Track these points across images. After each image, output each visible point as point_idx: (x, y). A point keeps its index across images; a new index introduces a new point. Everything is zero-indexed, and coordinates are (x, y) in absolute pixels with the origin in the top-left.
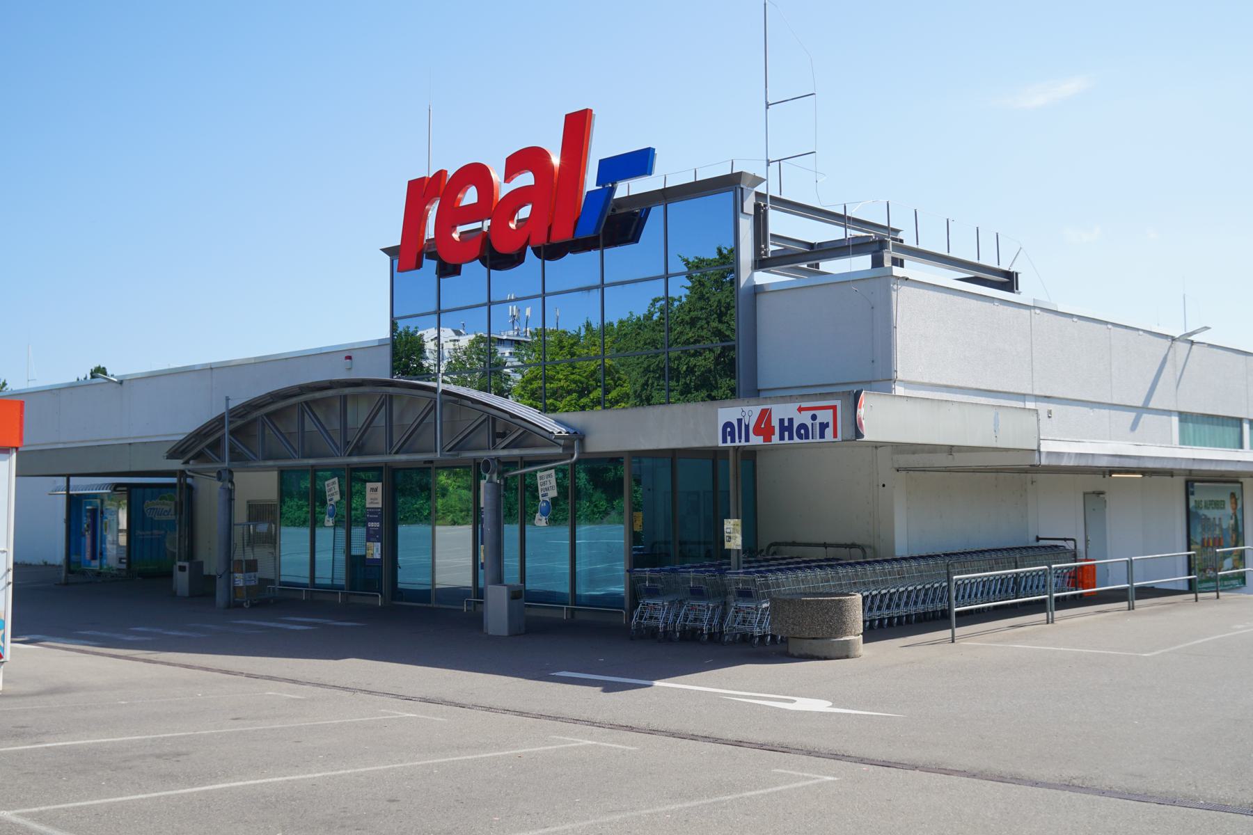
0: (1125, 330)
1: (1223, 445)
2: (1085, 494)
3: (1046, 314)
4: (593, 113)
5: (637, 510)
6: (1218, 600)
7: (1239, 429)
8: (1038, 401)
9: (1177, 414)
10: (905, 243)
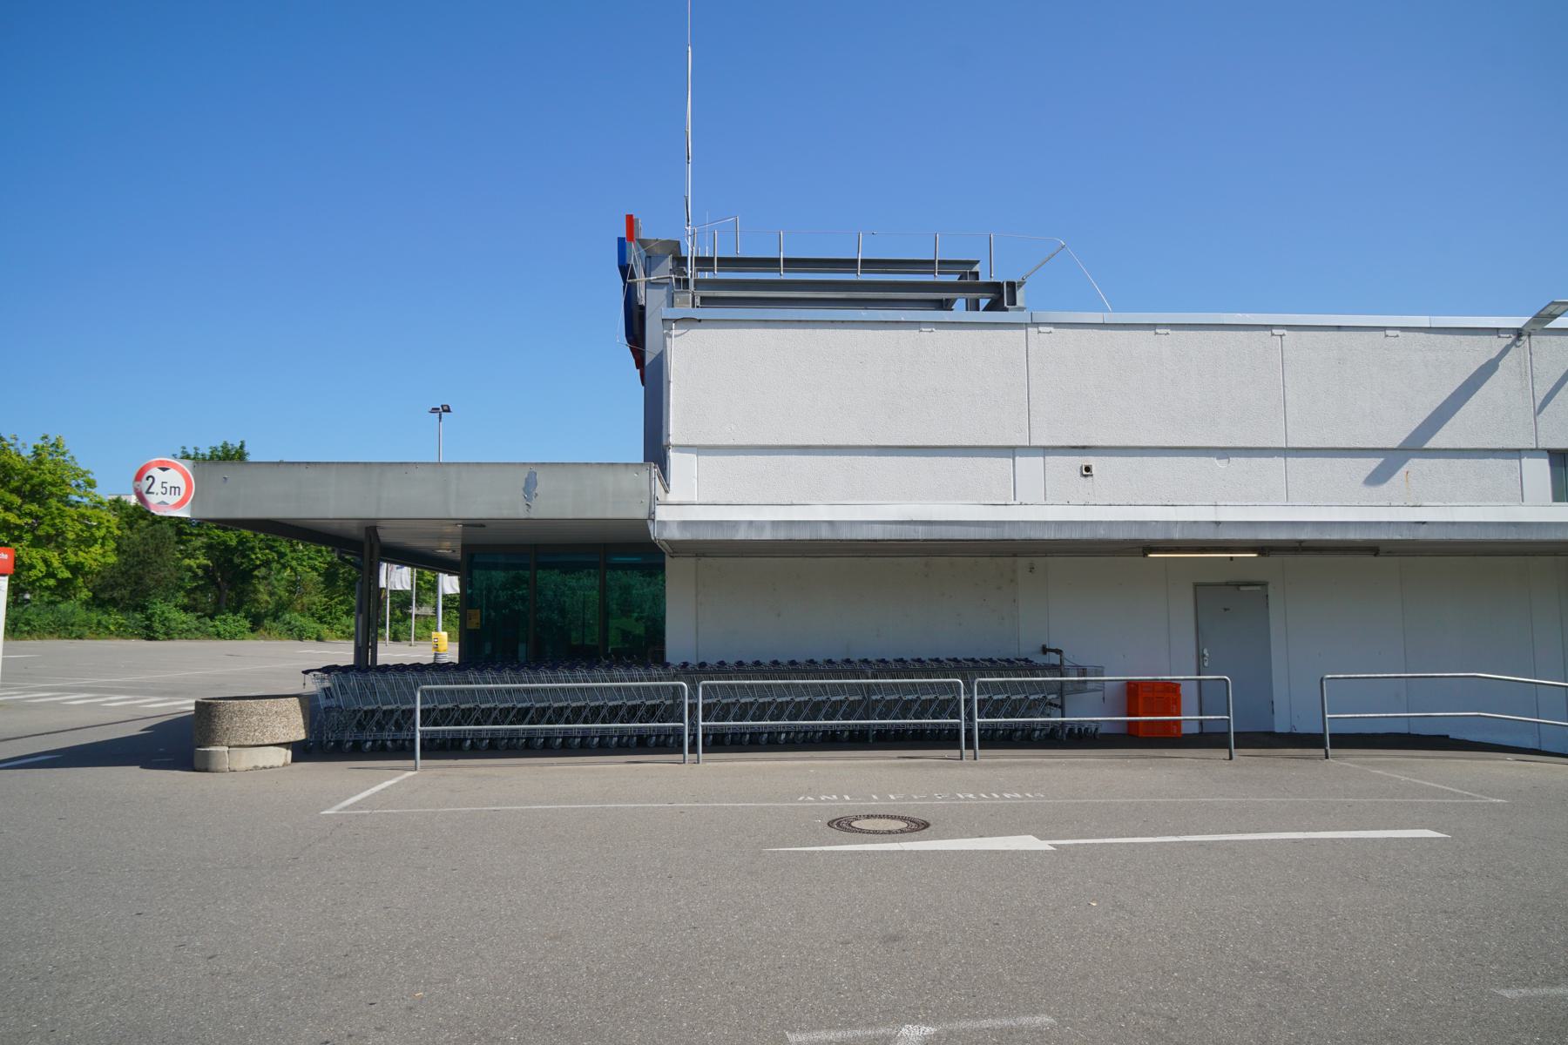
0: (1336, 333)
2: (1196, 586)
3: (1411, 335)
4: (634, 217)
5: (471, 607)
6: (1227, 763)
8: (701, 455)
9: (1546, 453)
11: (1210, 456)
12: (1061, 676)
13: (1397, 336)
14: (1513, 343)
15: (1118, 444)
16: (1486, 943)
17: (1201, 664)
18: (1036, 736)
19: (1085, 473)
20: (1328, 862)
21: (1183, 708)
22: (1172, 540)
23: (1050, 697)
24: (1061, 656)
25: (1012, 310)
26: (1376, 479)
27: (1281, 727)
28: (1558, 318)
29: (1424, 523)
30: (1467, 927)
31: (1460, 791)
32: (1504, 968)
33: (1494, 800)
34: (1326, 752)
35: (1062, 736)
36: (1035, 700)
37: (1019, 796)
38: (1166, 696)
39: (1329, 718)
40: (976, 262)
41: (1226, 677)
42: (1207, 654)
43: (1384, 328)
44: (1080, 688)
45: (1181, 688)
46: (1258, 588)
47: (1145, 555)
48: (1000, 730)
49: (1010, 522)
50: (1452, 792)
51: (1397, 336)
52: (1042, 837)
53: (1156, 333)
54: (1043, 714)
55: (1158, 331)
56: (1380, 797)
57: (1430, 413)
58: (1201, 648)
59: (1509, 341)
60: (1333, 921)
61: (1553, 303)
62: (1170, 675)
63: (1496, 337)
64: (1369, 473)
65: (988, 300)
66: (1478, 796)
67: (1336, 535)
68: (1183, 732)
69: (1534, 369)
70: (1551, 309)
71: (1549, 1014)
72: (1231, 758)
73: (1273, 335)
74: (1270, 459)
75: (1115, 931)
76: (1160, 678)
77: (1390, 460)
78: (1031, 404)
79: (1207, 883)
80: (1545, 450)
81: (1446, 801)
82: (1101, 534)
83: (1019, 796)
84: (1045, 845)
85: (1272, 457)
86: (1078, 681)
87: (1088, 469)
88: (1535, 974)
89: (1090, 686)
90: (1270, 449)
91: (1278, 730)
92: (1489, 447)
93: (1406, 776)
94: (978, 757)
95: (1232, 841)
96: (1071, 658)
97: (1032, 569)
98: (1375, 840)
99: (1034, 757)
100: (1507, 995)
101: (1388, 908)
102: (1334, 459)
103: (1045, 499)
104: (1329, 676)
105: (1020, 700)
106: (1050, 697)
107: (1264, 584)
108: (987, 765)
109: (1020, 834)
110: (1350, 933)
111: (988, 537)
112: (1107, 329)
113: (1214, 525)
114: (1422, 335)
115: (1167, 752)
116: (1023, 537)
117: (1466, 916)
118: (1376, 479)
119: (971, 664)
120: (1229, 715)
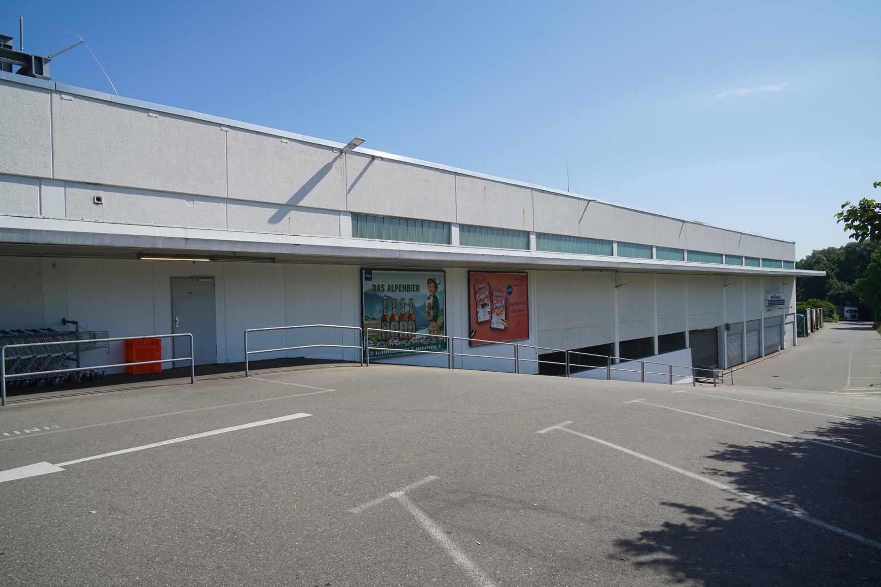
1: (434, 241)
2: (172, 278)
7: (650, 251)
10: (13, 50)
11: (182, 199)
12: (77, 340)
13: (287, 143)
14: (339, 157)
15: (121, 185)
16: (340, 479)
17: (174, 326)
18: (57, 381)
19: (96, 202)
20: (253, 444)
21: (163, 355)
22: (157, 249)
23: (68, 354)
24: (77, 325)
25: (39, 77)
26: (274, 220)
27: (220, 360)
28: (358, 147)
29: (299, 245)
30: (330, 471)
31: (314, 388)
32: (351, 493)
33: (329, 390)
34: (246, 373)
35: (77, 379)
36: (56, 357)
37: (37, 430)
38: (152, 347)
39: (248, 354)
40: (11, 38)
41: (190, 334)
42: (178, 320)
43: (281, 137)
44: (91, 347)
45: (161, 342)
46: (210, 280)
47: (139, 258)
48: (27, 380)
49: (34, 231)
50: (310, 389)
51: (287, 143)
52: (53, 462)
53: (149, 116)
54: (63, 366)
55: (150, 114)
56: (277, 397)
57: (301, 187)
58: (174, 316)
59: (337, 155)
60: (259, 486)
61: (356, 138)
62: (155, 335)
63: (332, 152)
64: (271, 216)
65: (20, 67)
66: (322, 389)
67: (254, 250)
68: (163, 369)
69: (347, 171)
70: (354, 142)
71: (376, 518)
72: (192, 383)
73: (221, 130)
74: (218, 204)
75: (110, 532)
76: (148, 337)
77: (282, 210)
78: (54, 148)
79: (179, 475)
80: (349, 212)
81: (308, 394)
82: (107, 242)
83: (37, 430)
84: (56, 468)
85: (219, 203)
86: (90, 342)
87: (99, 199)
88: (365, 493)
89: (98, 345)
90: (218, 198)
91: (219, 362)
92: (327, 208)
93: (287, 382)
94: (5, 403)
95: (195, 439)
96: (84, 326)
97: (54, 266)
98: (276, 424)
99: (54, 397)
100: (355, 512)
101: (288, 468)
102: (253, 208)
103: (66, 216)
104: (249, 330)
105: (44, 358)
106: (68, 354)
107: (213, 278)
108: (13, 409)
109: (36, 463)
110: (269, 491)
111: (15, 241)
112: (114, 106)
113: (184, 240)
114: (298, 144)
115: (152, 383)
116: (45, 242)
117: (328, 464)
118: (274, 220)
119: (17, 334)
120: (191, 357)
